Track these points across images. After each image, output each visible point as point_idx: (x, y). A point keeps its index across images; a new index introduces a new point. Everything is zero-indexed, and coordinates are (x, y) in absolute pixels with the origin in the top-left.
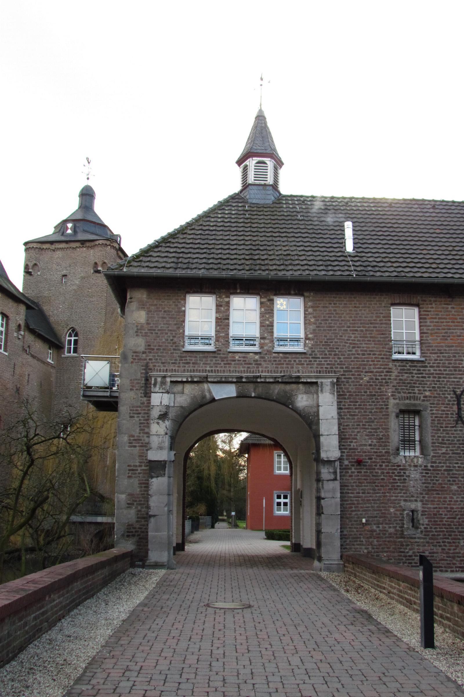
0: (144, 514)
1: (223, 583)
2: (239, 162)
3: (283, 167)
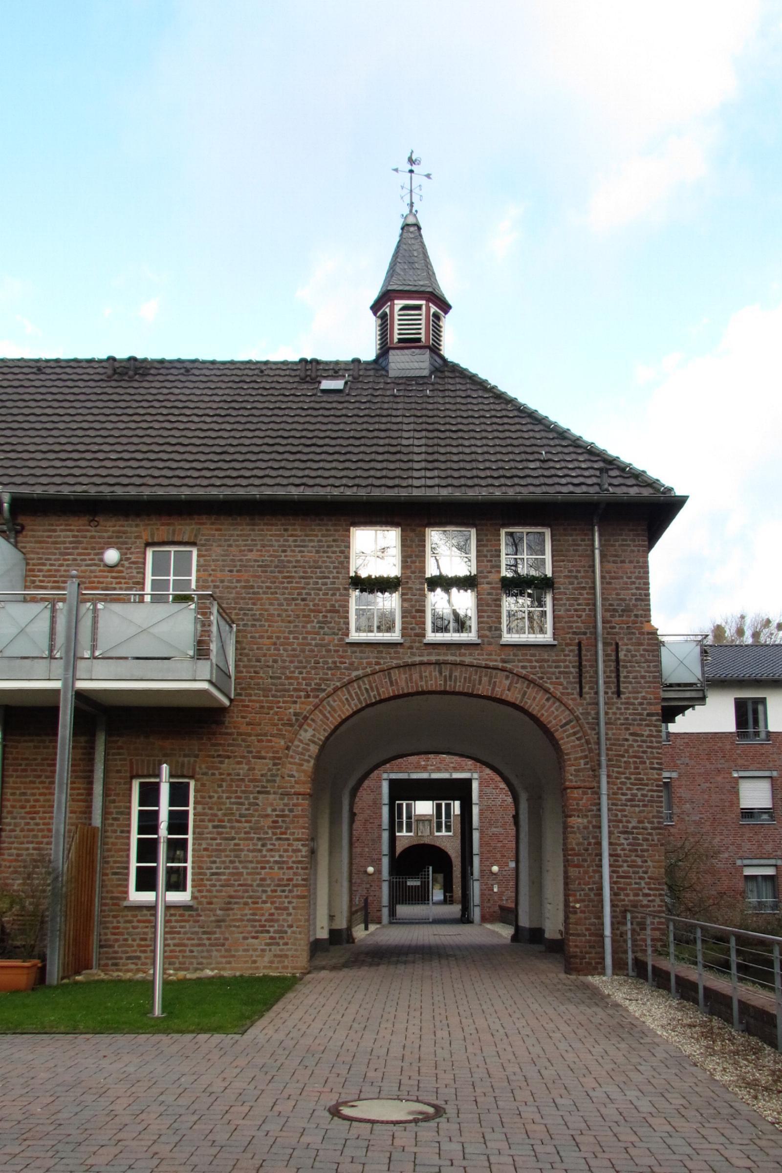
0: (627, 906)
1: (443, 1012)
2: (376, 307)
3: (451, 311)
